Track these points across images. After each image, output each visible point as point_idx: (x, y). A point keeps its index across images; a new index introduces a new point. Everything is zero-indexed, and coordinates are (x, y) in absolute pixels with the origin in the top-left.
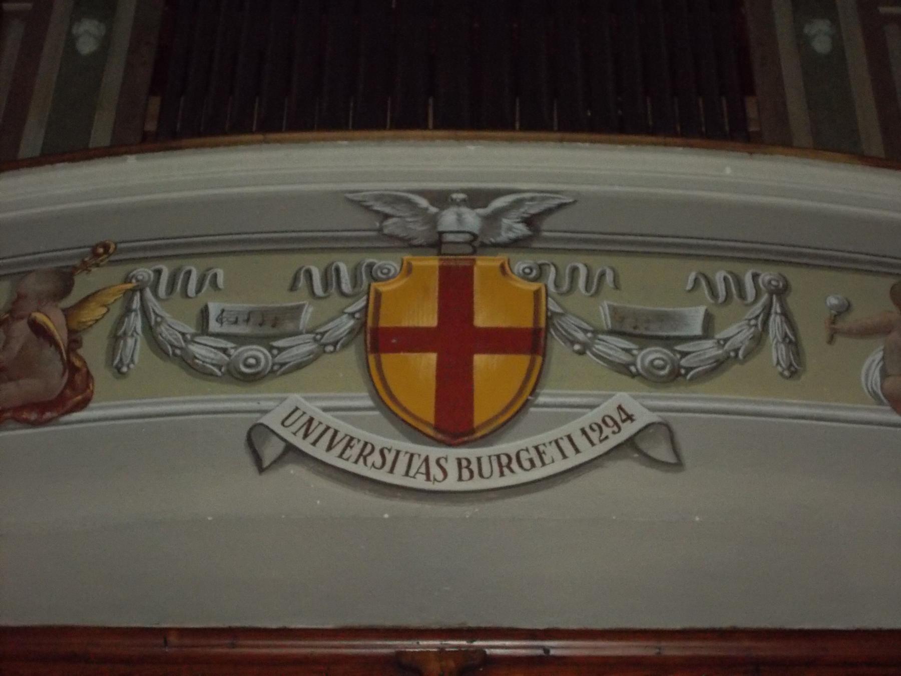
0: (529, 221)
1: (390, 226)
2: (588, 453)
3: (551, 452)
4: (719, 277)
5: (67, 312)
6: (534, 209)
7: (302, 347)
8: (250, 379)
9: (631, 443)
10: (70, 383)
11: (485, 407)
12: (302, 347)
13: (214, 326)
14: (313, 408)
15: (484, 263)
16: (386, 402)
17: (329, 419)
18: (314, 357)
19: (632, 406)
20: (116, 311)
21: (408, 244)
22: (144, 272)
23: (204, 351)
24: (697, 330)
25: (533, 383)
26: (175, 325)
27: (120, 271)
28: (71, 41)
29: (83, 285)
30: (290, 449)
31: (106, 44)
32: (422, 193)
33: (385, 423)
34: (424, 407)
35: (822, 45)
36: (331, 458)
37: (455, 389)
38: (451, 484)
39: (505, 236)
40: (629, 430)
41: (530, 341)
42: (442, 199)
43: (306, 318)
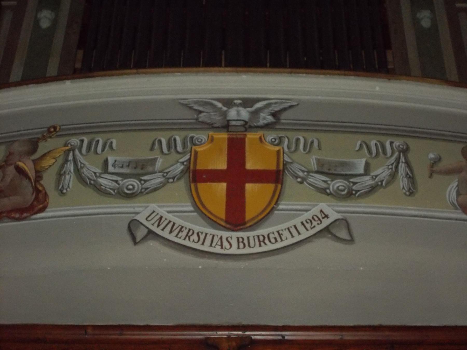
0: (274, 115)
1: (202, 117)
2: (305, 234)
3: (286, 234)
4: (372, 144)
5: (35, 162)
6: (277, 108)
7: (156, 180)
8: (130, 196)
9: (327, 229)
10: (37, 198)
11: (251, 211)
12: (156, 180)
13: (111, 169)
14: (162, 211)
15: (251, 136)
16: (200, 208)
17: (171, 217)
18: (163, 185)
19: (328, 210)
20: (60, 161)
21: (211, 127)
22: (75, 141)
23: (105, 182)
24: (362, 171)
25: (276, 198)
26: (91, 168)
27: (62, 140)
28: (37, 21)
29: (43, 148)
30: (150, 232)
31: (55, 23)
32: (219, 100)
33: (199, 219)
34: (220, 211)
35: (426, 23)
36: (172, 237)
37: (236, 201)
38: (234, 250)
39: (261, 122)
40: (326, 222)
41: (275, 177)
42: (229, 103)
43: (159, 165)
